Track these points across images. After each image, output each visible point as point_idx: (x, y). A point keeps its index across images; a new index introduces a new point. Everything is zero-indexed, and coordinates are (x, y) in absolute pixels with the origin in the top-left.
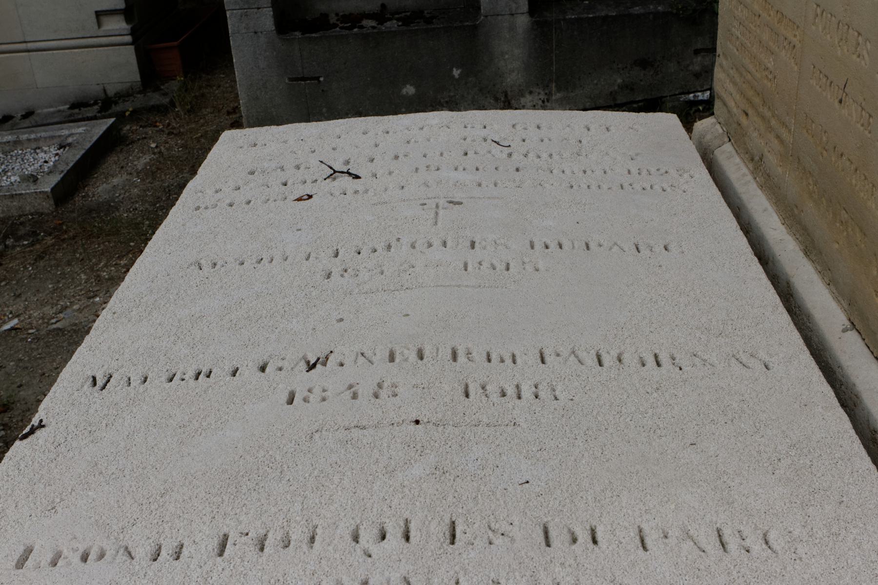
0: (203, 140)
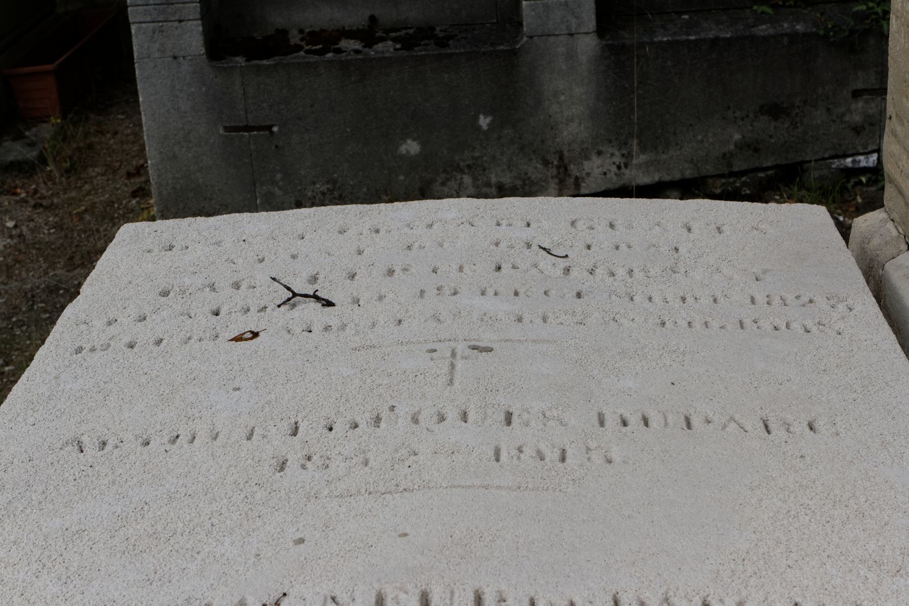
0: (88, 217)
